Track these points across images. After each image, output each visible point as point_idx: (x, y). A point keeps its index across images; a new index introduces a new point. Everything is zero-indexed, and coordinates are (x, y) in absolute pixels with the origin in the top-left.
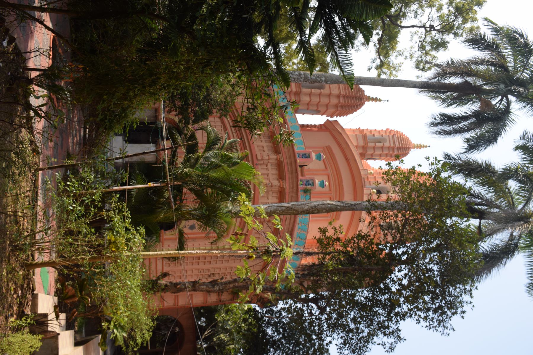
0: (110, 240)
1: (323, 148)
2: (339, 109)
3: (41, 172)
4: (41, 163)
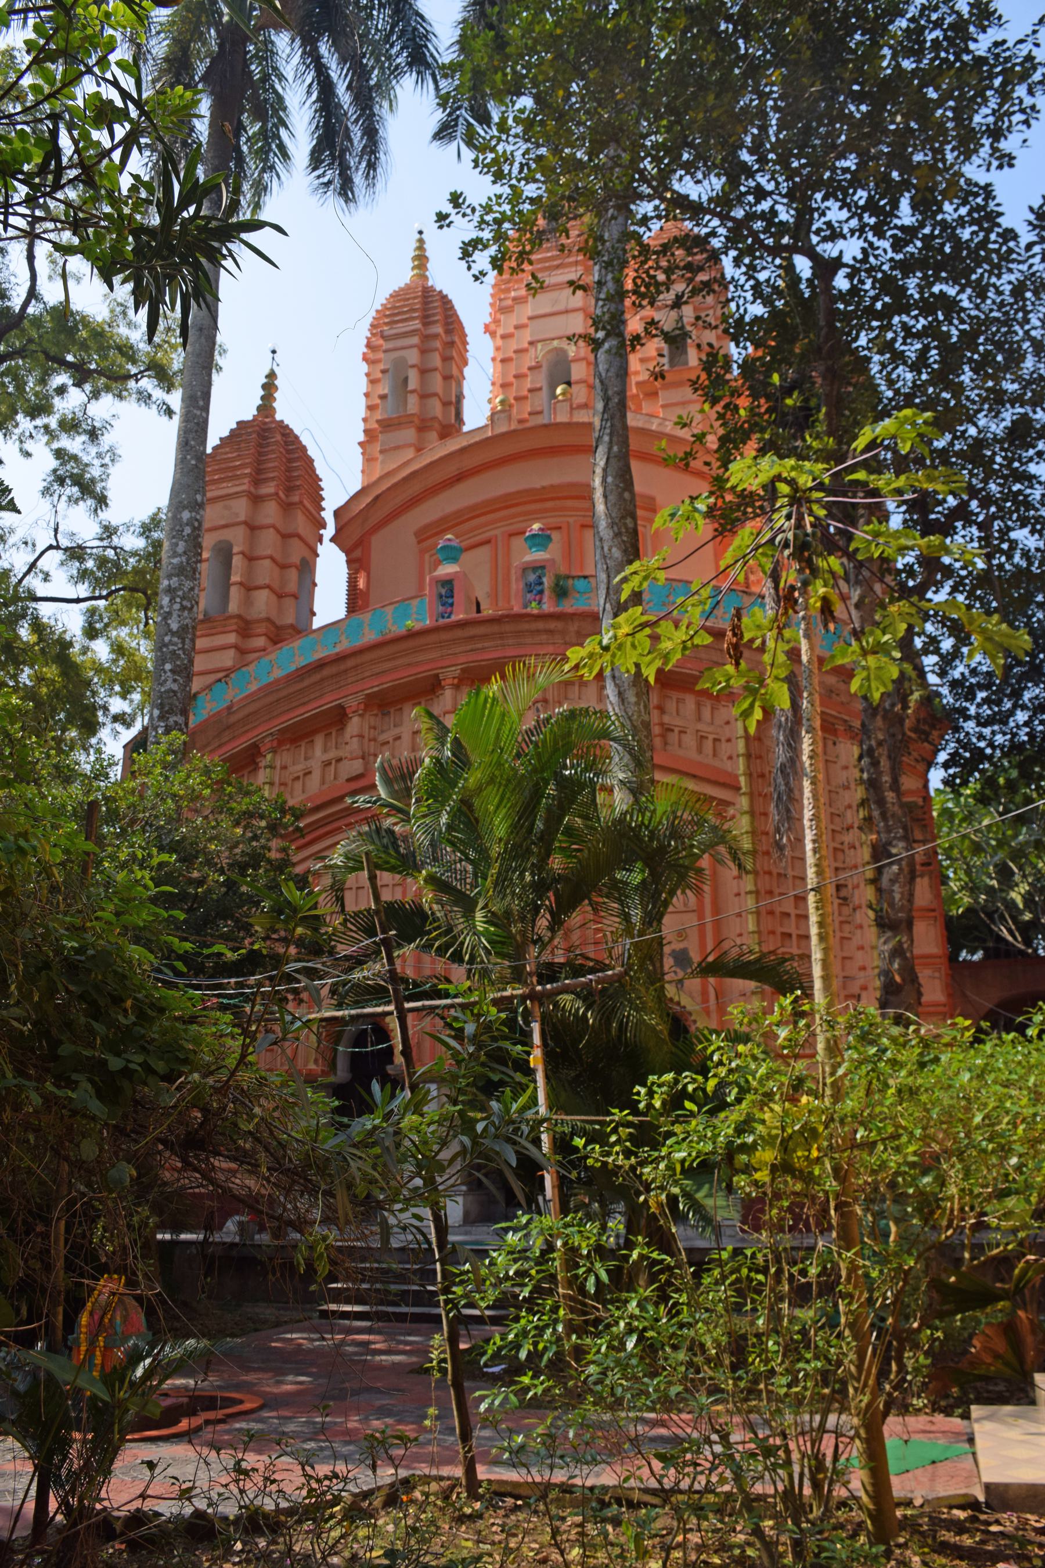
0: (774, 1168)
1: (422, 552)
2: (296, 499)
3: (483, 1472)
4: (445, 1471)
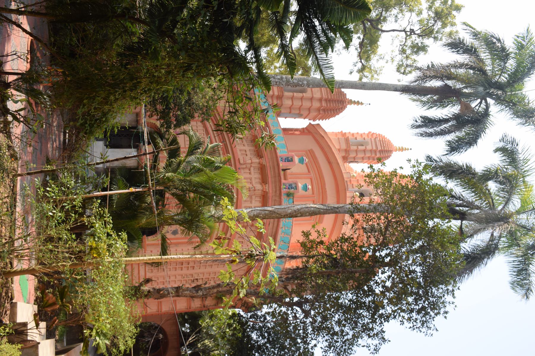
0: (91, 246)
1: (306, 152)
2: (321, 112)
4: (19, 169)
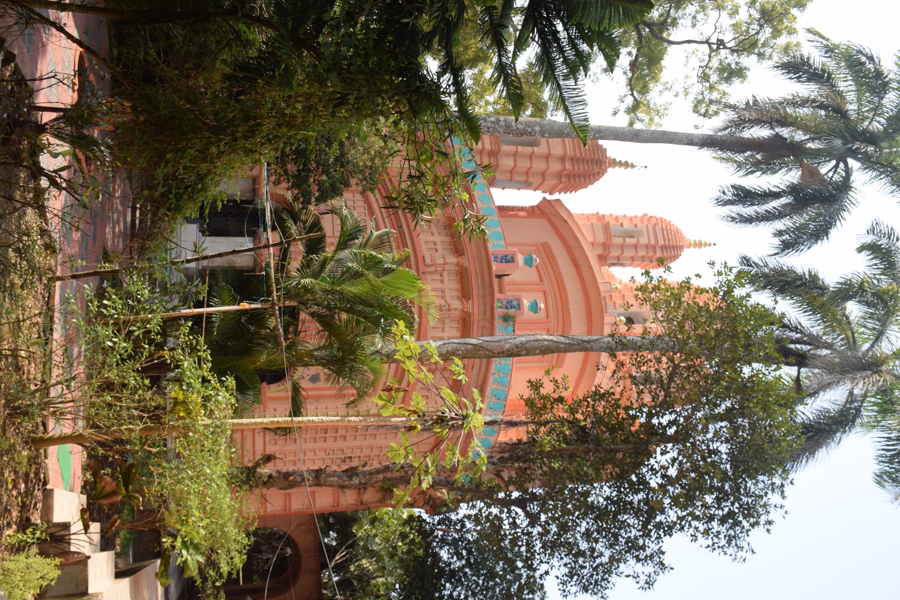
0: (176, 399)
2: (563, 179)
3: (58, 283)
